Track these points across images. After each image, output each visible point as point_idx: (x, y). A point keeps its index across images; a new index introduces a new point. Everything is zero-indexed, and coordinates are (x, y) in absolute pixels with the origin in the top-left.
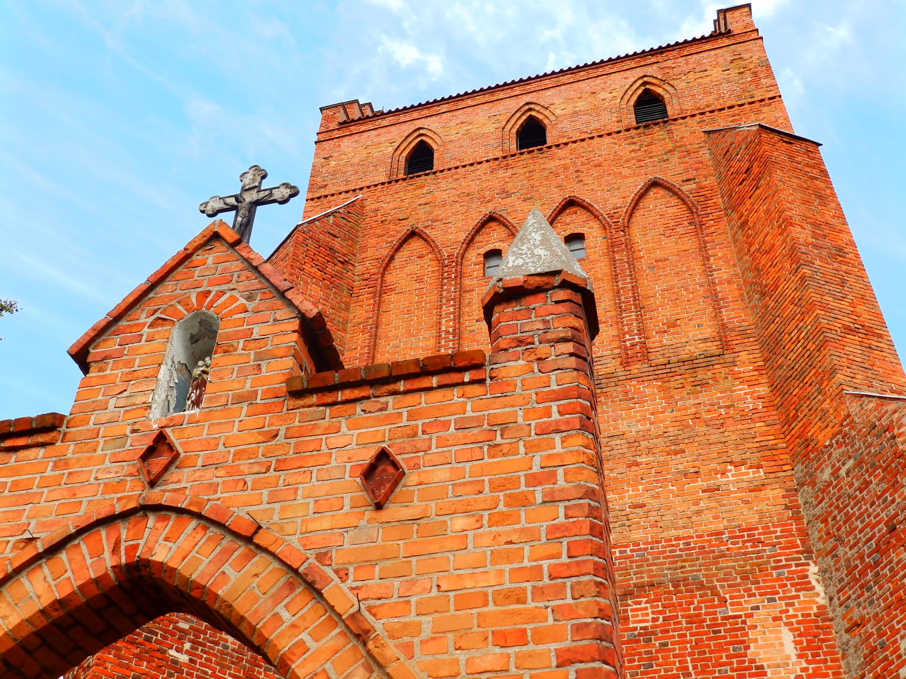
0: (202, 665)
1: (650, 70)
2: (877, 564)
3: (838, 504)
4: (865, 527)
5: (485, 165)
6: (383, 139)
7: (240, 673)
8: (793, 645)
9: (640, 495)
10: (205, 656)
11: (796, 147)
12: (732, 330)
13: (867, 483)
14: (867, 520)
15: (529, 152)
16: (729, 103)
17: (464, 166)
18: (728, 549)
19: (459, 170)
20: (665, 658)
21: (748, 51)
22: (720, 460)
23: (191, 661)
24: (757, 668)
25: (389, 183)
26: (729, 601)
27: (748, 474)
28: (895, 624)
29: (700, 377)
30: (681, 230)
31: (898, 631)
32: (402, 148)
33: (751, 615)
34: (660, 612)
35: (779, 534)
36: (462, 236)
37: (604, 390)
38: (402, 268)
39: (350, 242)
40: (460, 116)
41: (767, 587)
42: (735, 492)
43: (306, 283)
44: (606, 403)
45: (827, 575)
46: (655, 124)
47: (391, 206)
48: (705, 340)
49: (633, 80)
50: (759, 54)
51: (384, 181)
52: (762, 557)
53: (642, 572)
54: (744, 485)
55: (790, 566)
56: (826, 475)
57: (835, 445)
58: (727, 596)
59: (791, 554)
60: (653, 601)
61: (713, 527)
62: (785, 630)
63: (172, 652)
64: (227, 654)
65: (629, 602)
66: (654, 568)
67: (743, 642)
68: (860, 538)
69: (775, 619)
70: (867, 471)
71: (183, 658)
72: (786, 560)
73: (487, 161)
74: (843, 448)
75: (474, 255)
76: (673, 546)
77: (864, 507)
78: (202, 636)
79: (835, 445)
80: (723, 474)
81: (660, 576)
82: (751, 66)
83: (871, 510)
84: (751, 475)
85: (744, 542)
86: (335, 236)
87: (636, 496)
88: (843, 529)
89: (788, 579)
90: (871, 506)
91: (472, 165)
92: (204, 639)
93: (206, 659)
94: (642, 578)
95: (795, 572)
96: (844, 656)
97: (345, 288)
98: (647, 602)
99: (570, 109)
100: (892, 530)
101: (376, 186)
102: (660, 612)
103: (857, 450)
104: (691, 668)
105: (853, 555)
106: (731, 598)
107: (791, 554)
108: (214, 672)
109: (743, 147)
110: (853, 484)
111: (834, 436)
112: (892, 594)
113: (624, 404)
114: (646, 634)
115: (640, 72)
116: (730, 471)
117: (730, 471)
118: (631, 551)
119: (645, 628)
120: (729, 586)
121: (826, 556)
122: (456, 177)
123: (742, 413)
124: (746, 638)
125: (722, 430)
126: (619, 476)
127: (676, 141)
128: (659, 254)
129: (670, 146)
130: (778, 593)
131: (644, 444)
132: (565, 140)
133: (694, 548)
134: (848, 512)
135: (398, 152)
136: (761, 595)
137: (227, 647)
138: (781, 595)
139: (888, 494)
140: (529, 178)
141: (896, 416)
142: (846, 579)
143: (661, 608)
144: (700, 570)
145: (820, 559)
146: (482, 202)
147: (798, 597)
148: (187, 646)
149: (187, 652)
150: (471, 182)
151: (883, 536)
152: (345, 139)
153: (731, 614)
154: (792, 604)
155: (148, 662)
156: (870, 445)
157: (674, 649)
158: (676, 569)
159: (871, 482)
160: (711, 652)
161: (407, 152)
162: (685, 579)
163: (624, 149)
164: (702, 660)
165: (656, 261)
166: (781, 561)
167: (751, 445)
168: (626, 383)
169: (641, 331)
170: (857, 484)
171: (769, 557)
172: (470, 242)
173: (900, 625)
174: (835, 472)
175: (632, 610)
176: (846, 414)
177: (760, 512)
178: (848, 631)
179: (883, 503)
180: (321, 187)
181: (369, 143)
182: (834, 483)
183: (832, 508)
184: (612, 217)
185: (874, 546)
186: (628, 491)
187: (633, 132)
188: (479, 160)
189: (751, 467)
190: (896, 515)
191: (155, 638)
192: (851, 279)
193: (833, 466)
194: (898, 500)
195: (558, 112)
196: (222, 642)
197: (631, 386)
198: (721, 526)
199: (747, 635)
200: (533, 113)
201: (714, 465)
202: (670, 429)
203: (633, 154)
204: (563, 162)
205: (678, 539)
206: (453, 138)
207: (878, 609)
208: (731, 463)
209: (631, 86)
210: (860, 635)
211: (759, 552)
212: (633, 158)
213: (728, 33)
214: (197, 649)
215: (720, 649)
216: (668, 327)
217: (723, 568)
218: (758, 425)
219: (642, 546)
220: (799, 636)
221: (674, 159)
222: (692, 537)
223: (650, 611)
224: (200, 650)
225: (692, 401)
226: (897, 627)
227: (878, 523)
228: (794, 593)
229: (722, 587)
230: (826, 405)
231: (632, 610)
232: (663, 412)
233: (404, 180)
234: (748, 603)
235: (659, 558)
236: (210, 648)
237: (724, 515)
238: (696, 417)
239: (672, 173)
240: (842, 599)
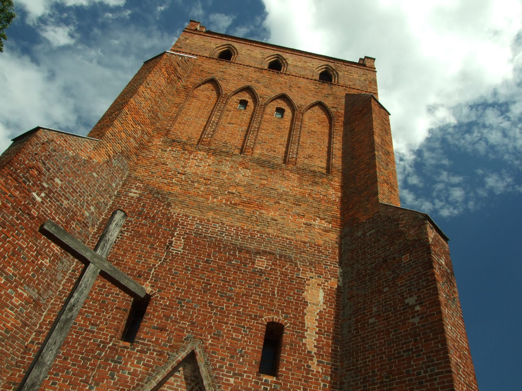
0: (46, 206)
1: (330, 64)
2: (372, 274)
3: (361, 247)
4: (372, 258)
5: (253, 68)
6: (213, 41)
7: (64, 219)
8: (323, 297)
9: (276, 216)
10: (50, 203)
11: (382, 110)
12: (335, 168)
13: (379, 241)
14: (374, 255)
15: (272, 71)
16: (358, 88)
17: (243, 65)
18: (307, 250)
19: (241, 66)
20: (266, 285)
21: (370, 76)
22: (315, 215)
23: (42, 202)
24: (305, 302)
25: (210, 58)
26: (301, 271)
27: (325, 224)
28: (224, 379)
29: (316, 180)
30: (325, 124)
31: (374, 303)
33: (309, 280)
34: (270, 265)
35: (330, 252)
36: (234, 89)
37: (274, 170)
38: (202, 91)
39: (184, 71)
40: (249, 47)
41: (319, 271)
42: (317, 229)
43: (160, 75)
44: (274, 175)
45: (346, 274)
46: (327, 83)
47: (207, 66)
48: (322, 168)
49: (323, 64)
50: (373, 77)
51: (207, 56)
52: (321, 258)
53: (267, 246)
54: (322, 228)
55: (331, 266)
56: (359, 234)
57: (368, 223)
58: (301, 269)
59: (333, 261)
60: (268, 260)
61: (303, 240)
62: (321, 291)
64: (61, 208)
65: (258, 256)
66: (273, 247)
67: (302, 289)
68: (368, 262)
69: (318, 285)
70: (380, 235)
71: (39, 199)
72: (330, 263)
73: (254, 67)
74: (371, 225)
75: (236, 98)
76: (284, 241)
77: (374, 250)
78: (52, 194)
79: (368, 223)
80: (315, 220)
81: (275, 251)
82: (370, 79)
83: (377, 252)
84: (326, 225)
85: (315, 250)
86: (179, 66)
87: (274, 216)
88: (360, 257)
89: (329, 271)
90: (377, 250)
91: (247, 66)
92: (52, 196)
93: (50, 205)
94: (267, 249)
95: (333, 269)
96: (343, 309)
97: (175, 87)
98: (265, 259)
99: (294, 63)
100: (385, 261)
101: (203, 56)
102: (270, 265)
103: (378, 226)
104: (276, 293)
105: (362, 268)
106: (303, 270)
107: (333, 261)
108: (51, 213)
109: (362, 102)
110: (371, 239)
111: (369, 219)
112: (375, 288)
113: (281, 178)
114: (260, 272)
116: (318, 220)
117: (318, 220)
118: (265, 236)
119: (261, 270)
120: (303, 265)
121: (348, 266)
122: (239, 67)
123: (329, 200)
124: (304, 288)
125: (319, 203)
126: (270, 205)
127: (333, 92)
128: (313, 129)
129: (330, 93)
130: (323, 275)
131: (284, 197)
132: (289, 73)
133: (293, 245)
134: (365, 250)
135: (217, 49)
136: (316, 273)
137: (62, 205)
138: (324, 276)
139: (387, 247)
140: (269, 80)
141: (402, 216)
142: (355, 278)
143: (271, 264)
144: (292, 254)
145: (345, 267)
146: (246, 81)
147: (330, 279)
148: (43, 195)
149: (42, 198)
150: (245, 72)
151: (380, 263)
152: (197, 35)
153: (300, 276)
154: (328, 282)
155: (20, 193)
156: (385, 225)
157: (271, 283)
158: (282, 250)
159: (381, 240)
160: (287, 289)
162: (285, 256)
163: (312, 87)
164: (282, 291)
165: (311, 131)
166: (328, 263)
167: (329, 214)
168: (284, 171)
169: (297, 154)
170: (373, 240)
171: (323, 259)
172: (236, 93)
173: (376, 301)
174: (364, 234)
175: (258, 260)
176: (377, 211)
177: (325, 241)
178: (348, 299)
179: (384, 249)
180: (179, 47)
181: (206, 41)
182: (362, 238)
183: (358, 248)
184: (299, 107)
185: (374, 266)
186: (272, 212)
187: (317, 82)
188: (250, 65)
189: (326, 222)
190: (389, 255)
191: (28, 183)
192: (390, 165)
193: (364, 231)
194: (392, 250)
195: (289, 62)
196: (60, 202)
197: (287, 173)
198: (307, 241)
199: (305, 287)
200: (279, 59)
201: (311, 216)
202: (297, 195)
203: (315, 89)
204: (285, 80)
205: (287, 239)
206: (242, 53)
207: (367, 293)
208: (319, 217)
209: (321, 66)
210: (354, 302)
211: (320, 256)
212: (314, 91)
213: (364, 65)
214: (47, 199)
215: (291, 289)
216: (308, 157)
217: (302, 257)
218: (334, 207)
219: (270, 236)
220: (327, 295)
221: (331, 98)
222: (293, 240)
223: (266, 263)
224: (48, 200)
225: (310, 188)
226: (374, 301)
227: (380, 257)
228: (329, 277)
229: (300, 264)
230: (368, 206)
231: (258, 260)
232: (297, 188)
233: (216, 59)
234: (309, 275)
235: (276, 244)
236: (53, 201)
237: (310, 237)
238: (310, 195)
239: (328, 102)
240: (350, 285)
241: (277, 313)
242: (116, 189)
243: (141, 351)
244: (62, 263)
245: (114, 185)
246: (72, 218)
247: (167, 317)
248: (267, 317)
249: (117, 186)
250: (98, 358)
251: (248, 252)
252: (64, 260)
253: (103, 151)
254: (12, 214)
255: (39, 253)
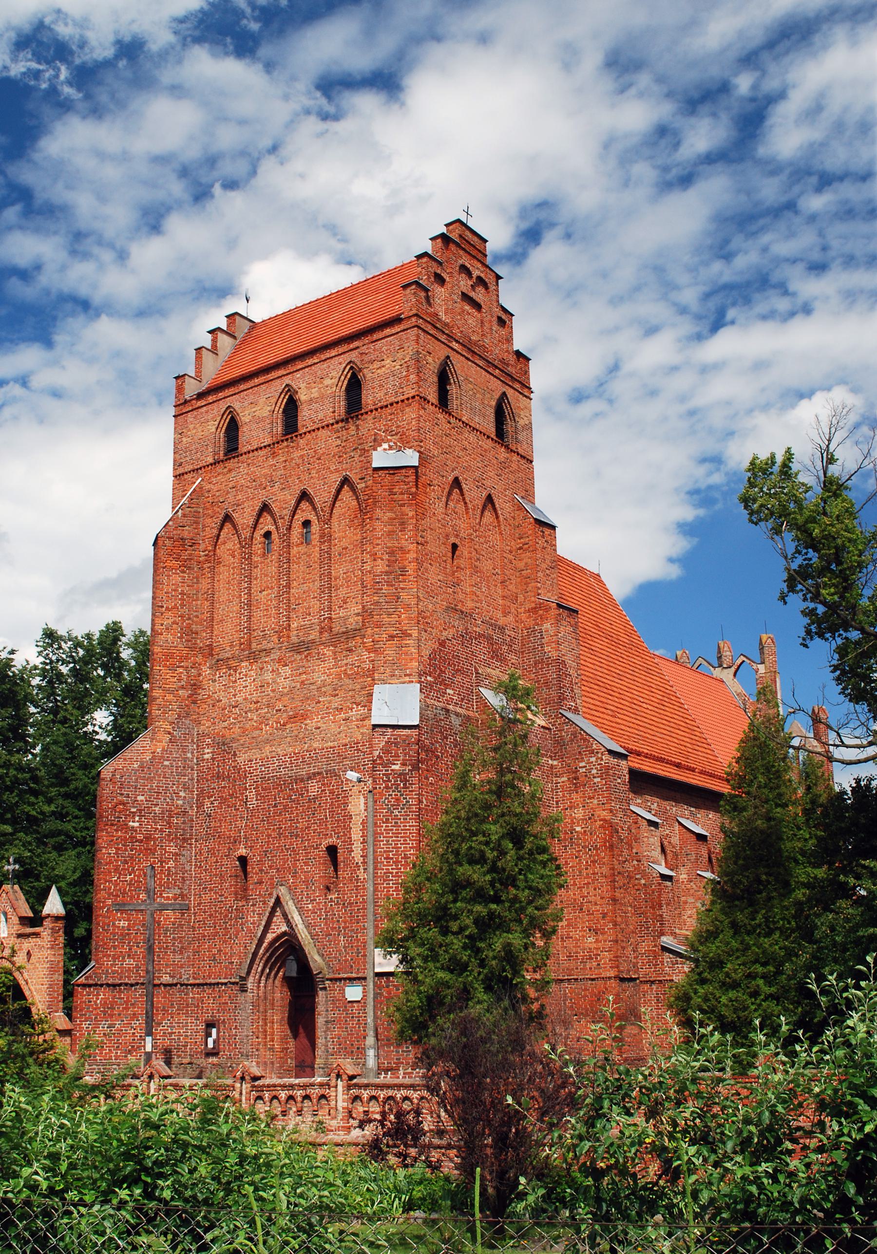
32: (221, 425)
43: (168, 576)
62: (362, 797)
63: (131, 824)
71: (136, 824)
115: (347, 358)
148: (137, 818)
152: (189, 414)
161: (224, 428)
225: (345, 662)
241: (331, 837)
242: (193, 756)
243: (253, 905)
244: (183, 855)
245: (189, 755)
246: (170, 816)
247: (261, 870)
248: (325, 843)
249: (192, 753)
250: (231, 919)
251: (302, 780)
252: (184, 853)
253: (159, 736)
254: (126, 850)
255: (162, 862)
